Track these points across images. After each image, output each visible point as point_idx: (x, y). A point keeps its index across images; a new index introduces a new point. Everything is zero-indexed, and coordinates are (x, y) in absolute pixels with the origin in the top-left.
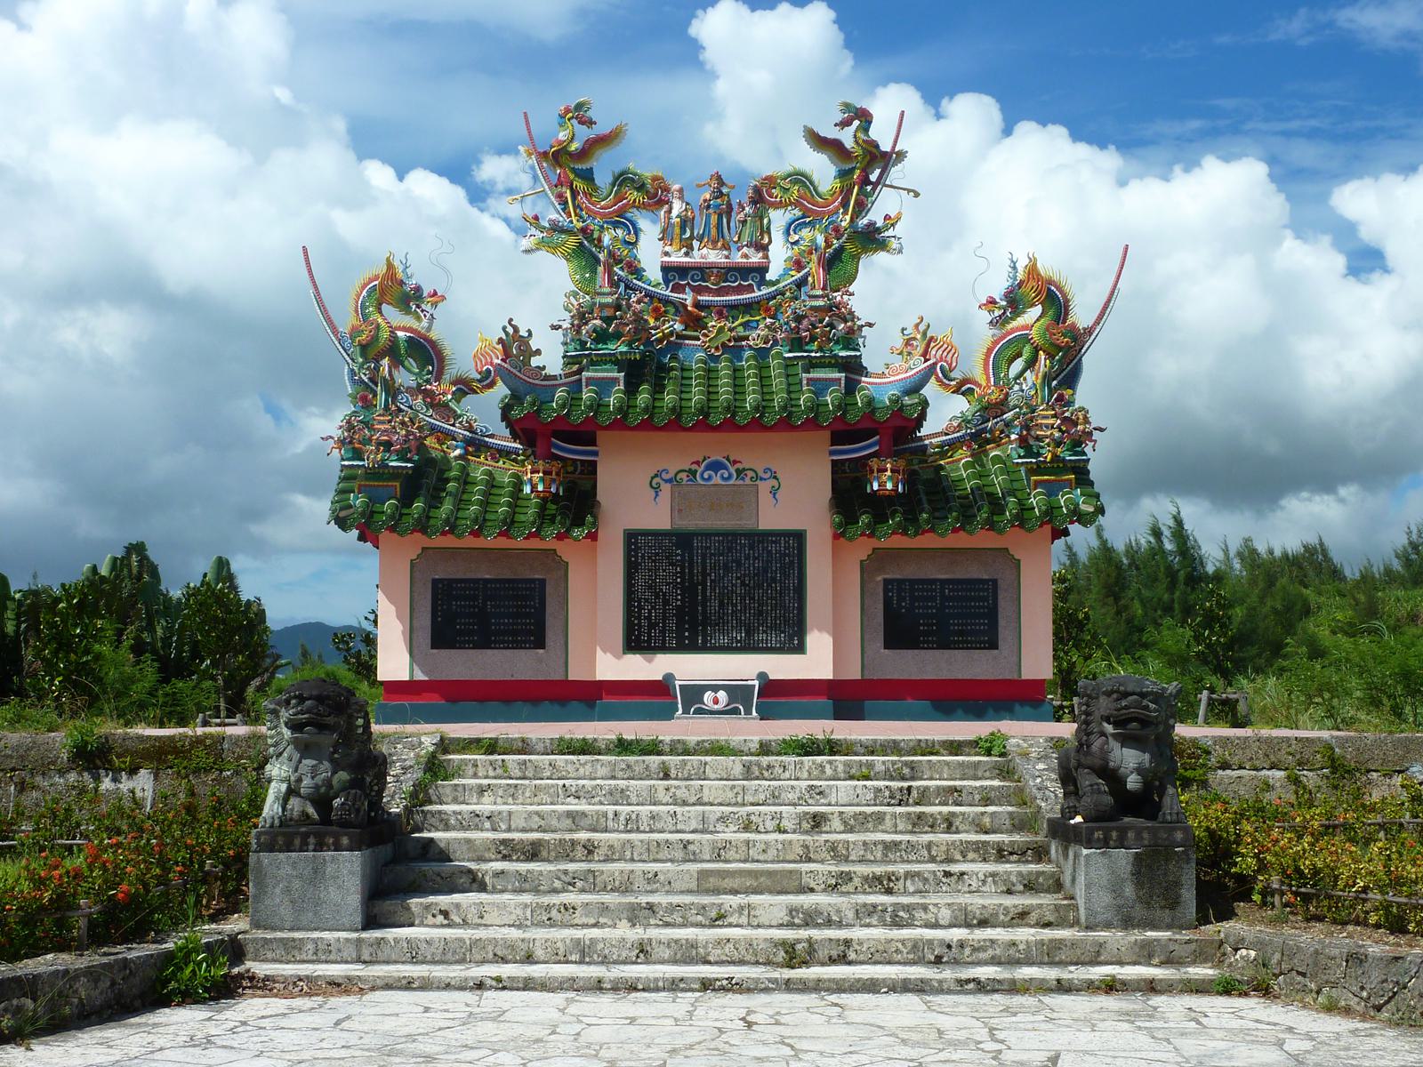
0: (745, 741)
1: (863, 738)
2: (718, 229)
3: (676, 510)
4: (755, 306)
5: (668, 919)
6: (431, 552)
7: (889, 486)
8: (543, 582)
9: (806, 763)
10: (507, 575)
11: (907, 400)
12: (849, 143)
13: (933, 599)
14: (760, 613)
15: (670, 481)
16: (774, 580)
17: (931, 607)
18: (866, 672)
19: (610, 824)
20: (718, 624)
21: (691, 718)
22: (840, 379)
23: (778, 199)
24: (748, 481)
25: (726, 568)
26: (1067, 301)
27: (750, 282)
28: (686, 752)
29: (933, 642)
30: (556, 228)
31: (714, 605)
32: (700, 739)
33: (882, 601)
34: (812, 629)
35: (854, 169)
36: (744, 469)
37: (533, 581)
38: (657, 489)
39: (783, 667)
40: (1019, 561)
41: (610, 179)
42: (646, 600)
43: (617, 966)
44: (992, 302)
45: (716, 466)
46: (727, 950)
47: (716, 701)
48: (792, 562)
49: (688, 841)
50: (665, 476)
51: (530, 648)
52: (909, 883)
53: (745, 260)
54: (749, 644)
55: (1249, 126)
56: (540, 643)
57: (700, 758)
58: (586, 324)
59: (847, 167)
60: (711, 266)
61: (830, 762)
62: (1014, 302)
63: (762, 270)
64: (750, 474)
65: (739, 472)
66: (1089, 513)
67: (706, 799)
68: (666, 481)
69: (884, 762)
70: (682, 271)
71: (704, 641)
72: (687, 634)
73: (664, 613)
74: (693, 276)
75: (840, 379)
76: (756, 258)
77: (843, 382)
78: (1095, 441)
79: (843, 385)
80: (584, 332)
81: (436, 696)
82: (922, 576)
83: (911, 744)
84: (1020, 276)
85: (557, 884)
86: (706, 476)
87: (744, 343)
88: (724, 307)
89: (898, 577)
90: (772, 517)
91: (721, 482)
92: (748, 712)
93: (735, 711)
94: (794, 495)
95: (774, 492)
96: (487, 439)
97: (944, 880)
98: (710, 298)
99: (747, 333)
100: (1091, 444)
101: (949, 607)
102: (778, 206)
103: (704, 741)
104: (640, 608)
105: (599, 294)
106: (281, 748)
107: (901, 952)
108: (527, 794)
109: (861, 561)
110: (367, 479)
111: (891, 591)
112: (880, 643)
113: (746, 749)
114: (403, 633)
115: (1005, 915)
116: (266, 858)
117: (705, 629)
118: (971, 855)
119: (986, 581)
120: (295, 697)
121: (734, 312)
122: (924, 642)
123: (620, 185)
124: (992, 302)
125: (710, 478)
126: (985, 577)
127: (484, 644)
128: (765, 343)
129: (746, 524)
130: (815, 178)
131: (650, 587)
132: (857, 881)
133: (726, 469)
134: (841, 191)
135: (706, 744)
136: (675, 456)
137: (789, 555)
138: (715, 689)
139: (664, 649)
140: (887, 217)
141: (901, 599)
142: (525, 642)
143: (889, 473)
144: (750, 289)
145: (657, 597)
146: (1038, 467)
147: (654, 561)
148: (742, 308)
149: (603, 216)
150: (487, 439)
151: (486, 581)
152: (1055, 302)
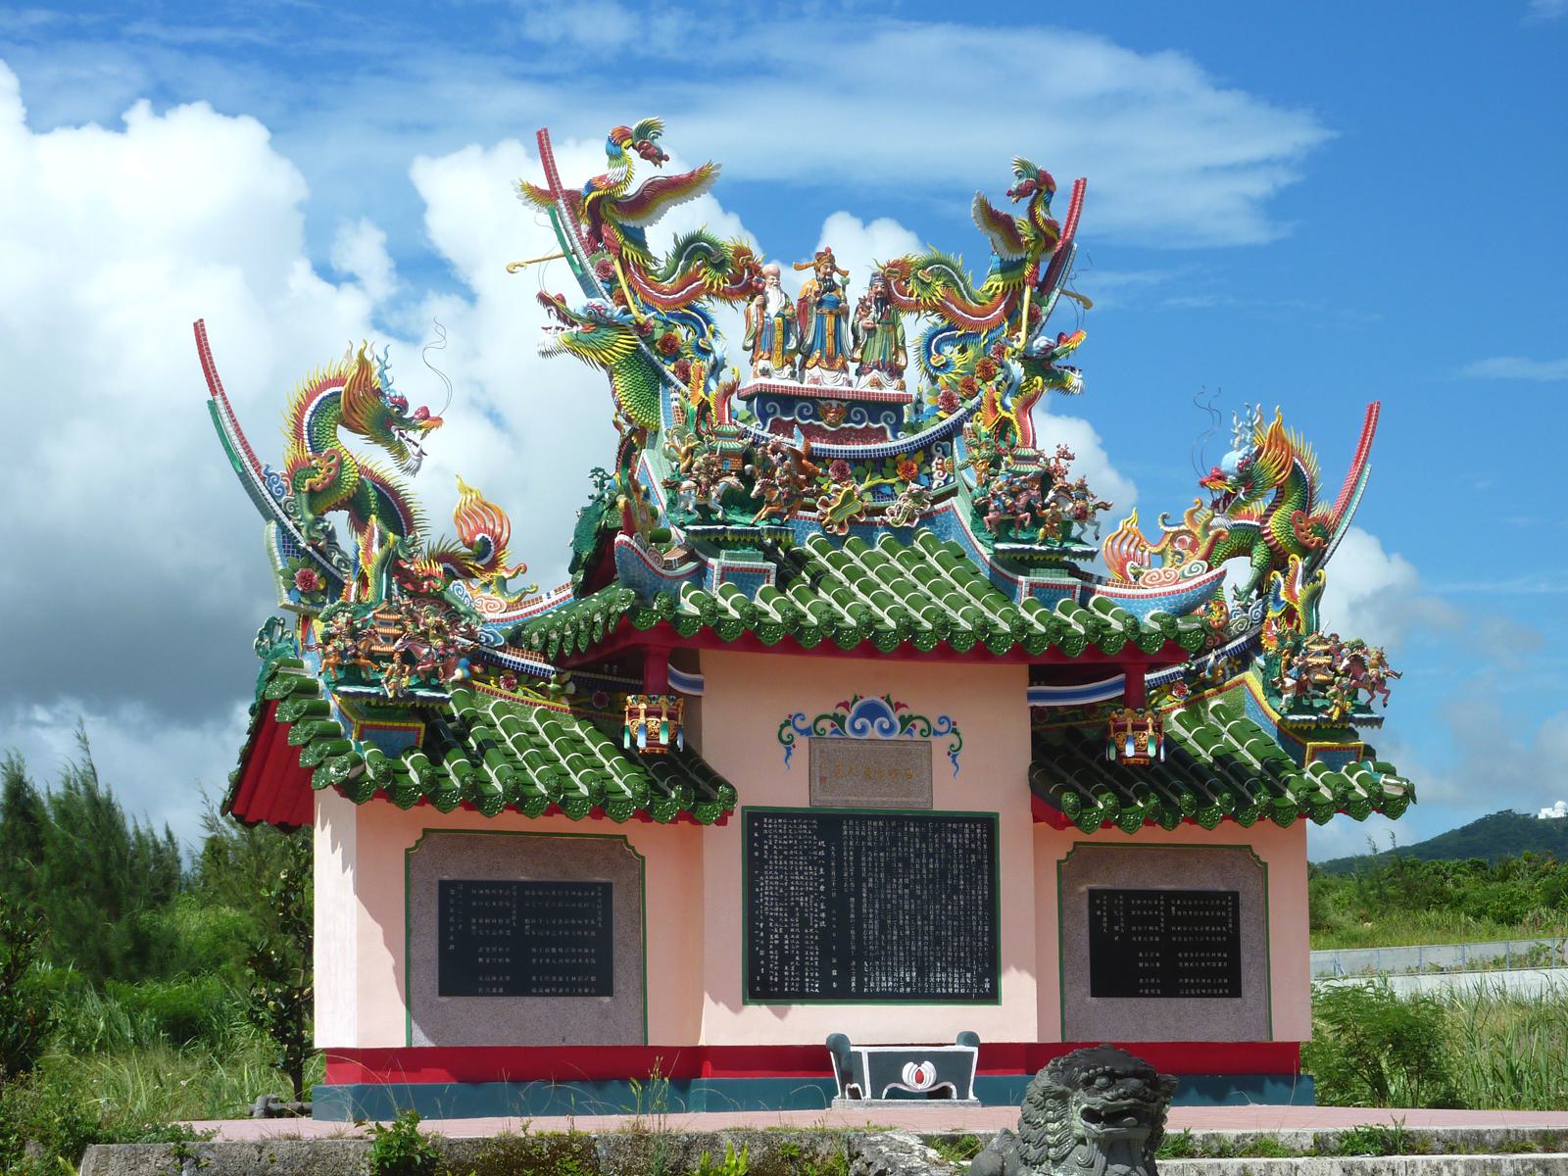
0: (1297, 1135)
1: (1440, 1129)
2: (835, 337)
3: (818, 778)
4: (889, 462)
6: (435, 836)
7: (1151, 751)
8: (607, 888)
9: (1419, 1165)
10: (553, 875)
11: (1181, 624)
13: (1155, 921)
14: (938, 941)
15: (806, 732)
16: (955, 890)
17: (1154, 933)
18: (1068, 1033)
20: (878, 958)
21: (881, 1105)
22: (1074, 587)
23: (914, 299)
24: (916, 736)
25: (890, 871)
27: (883, 424)
28: (1223, 1153)
29: (1155, 986)
30: (597, 320)
31: (872, 928)
32: (1240, 1132)
33: (1087, 923)
34: (1008, 967)
35: (1024, 261)
36: (911, 718)
37: (594, 885)
38: (788, 744)
40: (1265, 864)
41: (671, 248)
42: (776, 919)
45: (871, 711)
47: (920, 1078)
48: (979, 863)
50: (801, 725)
51: (590, 994)
53: (876, 390)
54: (923, 988)
55: (137, 28)
57: (1289, 1159)
58: (715, 481)
59: (1017, 257)
60: (831, 397)
61: (1448, 1163)
65: (904, 721)
66: (1395, 799)
68: (802, 732)
69: (1512, 1162)
70: (787, 400)
71: (860, 984)
72: (834, 973)
73: (802, 939)
74: (802, 408)
75: (1074, 587)
77: (1078, 591)
78: (1388, 692)
79: (1077, 596)
80: (714, 494)
81: (443, 1072)
82: (1139, 886)
83: (1498, 1136)
86: (858, 725)
87: (877, 519)
88: (846, 460)
89: (1108, 886)
90: (952, 792)
92: (963, 1095)
93: (943, 1094)
94: (980, 762)
95: (953, 753)
96: (500, 654)
98: (828, 446)
99: (882, 504)
101: (1176, 933)
102: (916, 307)
103: (1245, 1136)
104: (767, 931)
105: (719, 435)
106: (1066, 1148)
109: (1059, 862)
110: (370, 716)
111: (1100, 907)
113: (1297, 1146)
114: (395, 969)
117: (859, 967)
119: (1223, 895)
120: (1104, 1074)
121: (860, 470)
122: (1144, 986)
123: (690, 258)
125: (864, 729)
126: (1222, 888)
127: (519, 987)
128: (908, 521)
129: (914, 802)
131: (781, 899)
133: (885, 714)
134: (1004, 295)
135: (1248, 1140)
137: (975, 851)
138: (918, 1058)
139: (803, 996)
141: (1113, 920)
142: (583, 985)
143: (1150, 732)
144: (880, 435)
145: (792, 914)
146: (1318, 727)
147: (786, 858)
148: (869, 464)
149: (667, 304)
150: (500, 654)
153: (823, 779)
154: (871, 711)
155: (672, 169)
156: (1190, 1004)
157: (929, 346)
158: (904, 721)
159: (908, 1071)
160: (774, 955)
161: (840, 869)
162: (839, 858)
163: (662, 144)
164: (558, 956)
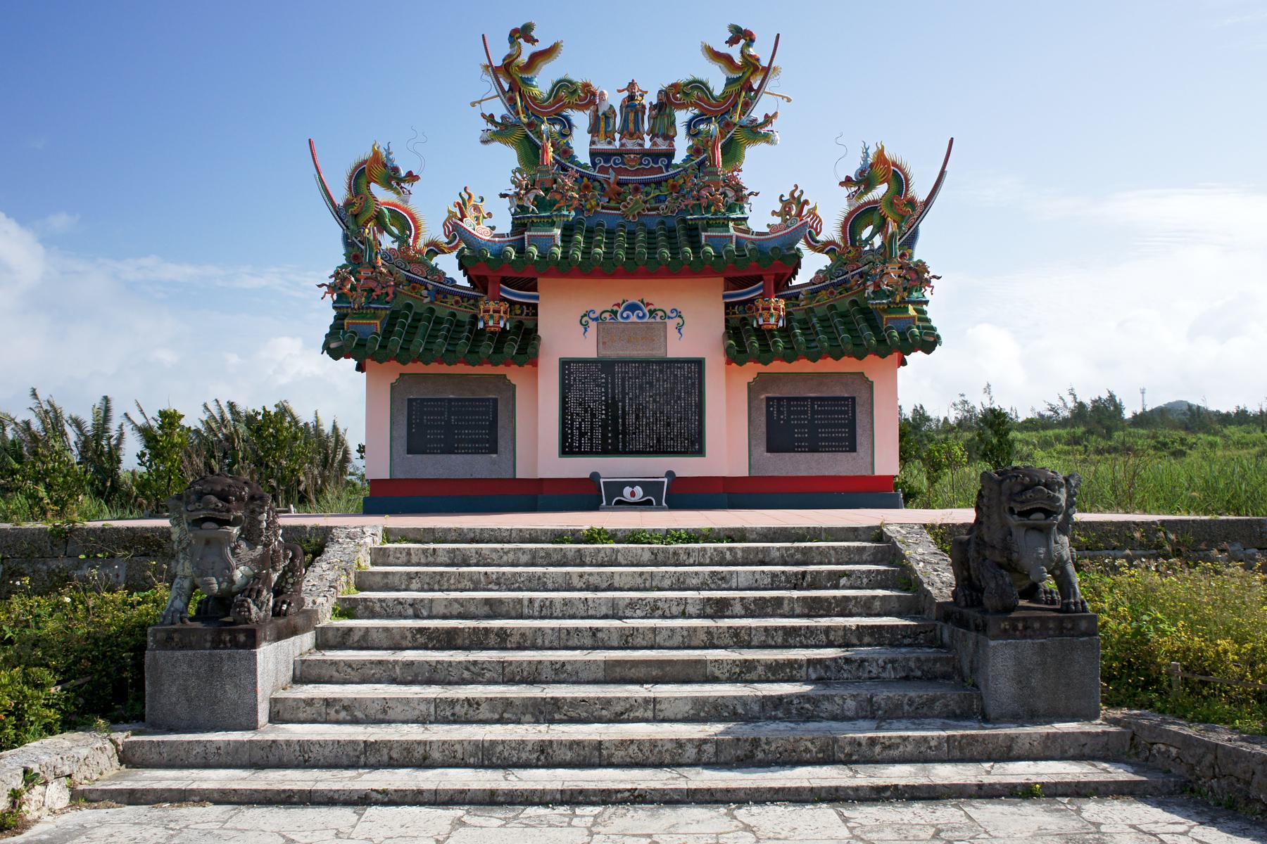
5: (573, 714)
8: (495, 401)
12: (738, 59)
13: (805, 413)
14: (669, 424)
15: (596, 319)
16: (679, 398)
19: (526, 611)
24: (658, 319)
26: (907, 180)
38: (586, 326)
39: (686, 467)
43: (516, 771)
44: (848, 179)
45: (633, 308)
46: (631, 752)
47: (633, 494)
48: (693, 384)
49: (597, 629)
50: (592, 315)
52: (811, 670)
56: (494, 450)
61: (730, 549)
62: (864, 180)
63: (670, 155)
64: (660, 314)
65: (651, 312)
67: (616, 585)
70: (607, 155)
76: (662, 145)
84: (870, 161)
85: (466, 675)
89: (778, 395)
90: (677, 348)
91: (635, 319)
93: (649, 503)
94: (693, 326)
97: (845, 667)
100: (929, 289)
104: (572, 420)
107: (810, 751)
108: (452, 581)
112: (763, 448)
115: (910, 705)
116: (161, 655)
118: (867, 639)
119: (846, 399)
124: (848, 179)
125: (628, 317)
129: (657, 353)
130: (711, 86)
132: (760, 669)
136: (603, 297)
138: (632, 485)
140: (766, 116)
141: (780, 413)
145: (586, 412)
151: (450, 400)
152: (899, 180)
153: (604, 343)
154: (633, 308)
155: (539, 47)
156: (825, 456)
157: (691, 125)
158: (651, 312)
159: (627, 491)
160: (576, 432)
161: (613, 389)
162: (613, 383)
163: (534, 34)
164: (469, 434)
